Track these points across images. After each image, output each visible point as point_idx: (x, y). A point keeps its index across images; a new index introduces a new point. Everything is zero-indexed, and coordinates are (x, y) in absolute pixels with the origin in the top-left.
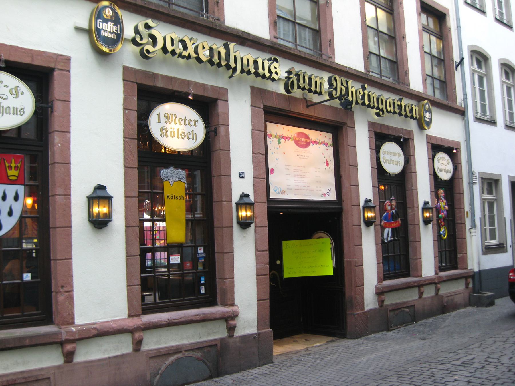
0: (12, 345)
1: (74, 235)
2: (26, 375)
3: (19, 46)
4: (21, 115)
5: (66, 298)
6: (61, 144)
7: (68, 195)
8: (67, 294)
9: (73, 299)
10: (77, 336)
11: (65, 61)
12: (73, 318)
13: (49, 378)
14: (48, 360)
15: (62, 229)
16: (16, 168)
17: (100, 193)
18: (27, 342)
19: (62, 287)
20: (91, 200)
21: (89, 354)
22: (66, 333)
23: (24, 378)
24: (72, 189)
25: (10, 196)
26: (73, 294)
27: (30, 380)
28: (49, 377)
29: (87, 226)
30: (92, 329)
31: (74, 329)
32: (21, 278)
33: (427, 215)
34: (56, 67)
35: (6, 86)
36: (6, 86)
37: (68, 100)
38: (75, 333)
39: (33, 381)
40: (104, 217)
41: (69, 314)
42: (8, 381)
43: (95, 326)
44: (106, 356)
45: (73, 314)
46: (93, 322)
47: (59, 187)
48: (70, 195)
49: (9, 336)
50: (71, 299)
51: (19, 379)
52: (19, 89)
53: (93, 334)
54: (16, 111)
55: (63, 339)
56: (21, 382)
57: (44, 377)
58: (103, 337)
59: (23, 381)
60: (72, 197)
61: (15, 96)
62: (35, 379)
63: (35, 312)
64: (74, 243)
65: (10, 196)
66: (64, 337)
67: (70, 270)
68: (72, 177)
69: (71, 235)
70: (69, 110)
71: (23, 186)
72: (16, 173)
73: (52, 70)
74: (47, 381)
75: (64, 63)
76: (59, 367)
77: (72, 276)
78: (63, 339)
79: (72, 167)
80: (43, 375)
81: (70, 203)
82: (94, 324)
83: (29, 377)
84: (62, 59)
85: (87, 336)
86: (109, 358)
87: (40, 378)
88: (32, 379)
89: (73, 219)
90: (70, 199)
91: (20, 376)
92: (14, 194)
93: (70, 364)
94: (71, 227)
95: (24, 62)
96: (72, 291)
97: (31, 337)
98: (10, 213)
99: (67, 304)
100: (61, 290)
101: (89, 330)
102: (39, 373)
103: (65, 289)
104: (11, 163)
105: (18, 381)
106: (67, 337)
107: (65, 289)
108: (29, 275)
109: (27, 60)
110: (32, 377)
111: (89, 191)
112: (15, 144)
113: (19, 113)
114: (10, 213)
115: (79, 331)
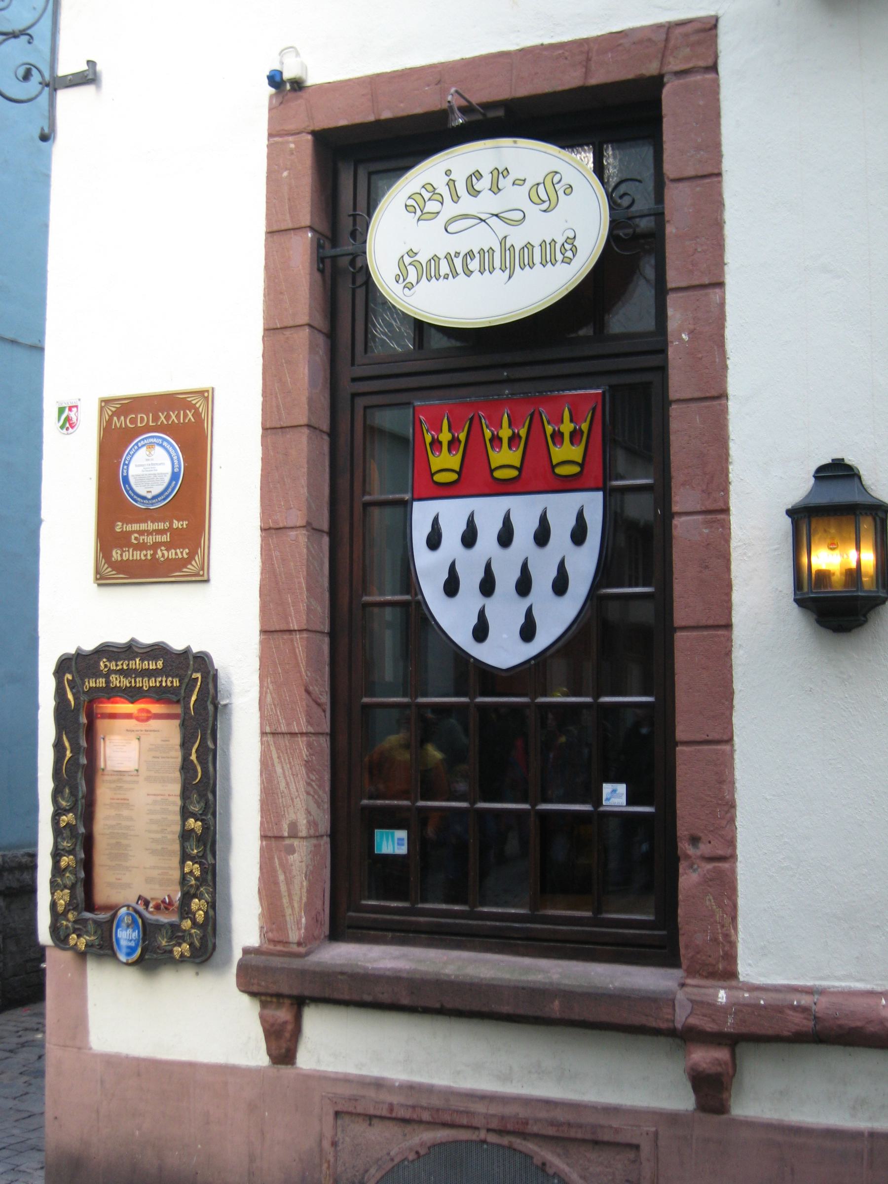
0: (506, 1009)
1: (739, 656)
2: (560, 1115)
3: (547, 41)
4: (567, 261)
5: (707, 881)
6: (691, 333)
7: (718, 512)
8: (710, 866)
9: (733, 889)
10: (730, 1025)
11: (694, 38)
12: (731, 957)
13: (637, 1147)
14: (641, 1086)
15: (695, 634)
16: (575, 436)
17: (839, 494)
18: (555, 1008)
19: (695, 840)
20: (807, 519)
21: (782, 1097)
22: (689, 1006)
23: (552, 1123)
24: (732, 488)
25: (561, 530)
26: (733, 871)
27: (573, 1134)
28: (634, 1141)
29: (795, 622)
30: (795, 1008)
31: (722, 996)
32: (598, 799)
33: (831, 558)
34: (666, 69)
35: (519, 182)
36: (519, 182)
37: (716, 171)
38: (724, 1010)
39: (584, 1141)
40: (846, 584)
41: (715, 940)
42: (503, 1118)
43: (806, 1000)
44: (862, 1123)
45: (733, 945)
46: (810, 983)
47: (683, 484)
48: (726, 511)
49: (507, 976)
50: (725, 887)
51: (537, 1121)
52: (557, 178)
53: (794, 1028)
54: (554, 252)
55: (679, 1026)
56: (544, 1132)
57: (620, 1138)
58: (850, 1049)
59: (551, 1131)
60: (733, 519)
61: (545, 206)
62: (588, 1136)
63: (444, 906)
64: (738, 685)
65: (561, 530)
66: (681, 1017)
67: (722, 782)
68: (731, 445)
69: (729, 653)
70: (718, 204)
71: (600, 495)
72: (575, 453)
73: (657, 82)
74: (632, 1155)
75: (692, 45)
76: (672, 1118)
77: (732, 805)
78: (679, 1026)
79: (733, 406)
80: (617, 1131)
81: (726, 538)
82: (809, 991)
83: (570, 1125)
84: (686, 35)
85: (771, 1032)
86: (873, 1135)
87: (606, 1138)
88: (579, 1135)
89: (736, 596)
90: (726, 526)
91: (543, 1114)
92: (571, 522)
93: (717, 1118)
94: (728, 626)
95: (560, 88)
96: (732, 857)
97: (568, 995)
98: (560, 586)
99: (710, 901)
100: (691, 851)
101: (779, 1009)
102: (603, 1121)
103: (704, 849)
104: (440, 430)
105: (535, 1129)
106: (692, 1021)
107: (704, 849)
108: (622, 788)
109: (571, 79)
110: (580, 1126)
111: (799, 487)
112: (617, 356)
113: (559, 257)
114: (560, 586)
115: (738, 1008)
